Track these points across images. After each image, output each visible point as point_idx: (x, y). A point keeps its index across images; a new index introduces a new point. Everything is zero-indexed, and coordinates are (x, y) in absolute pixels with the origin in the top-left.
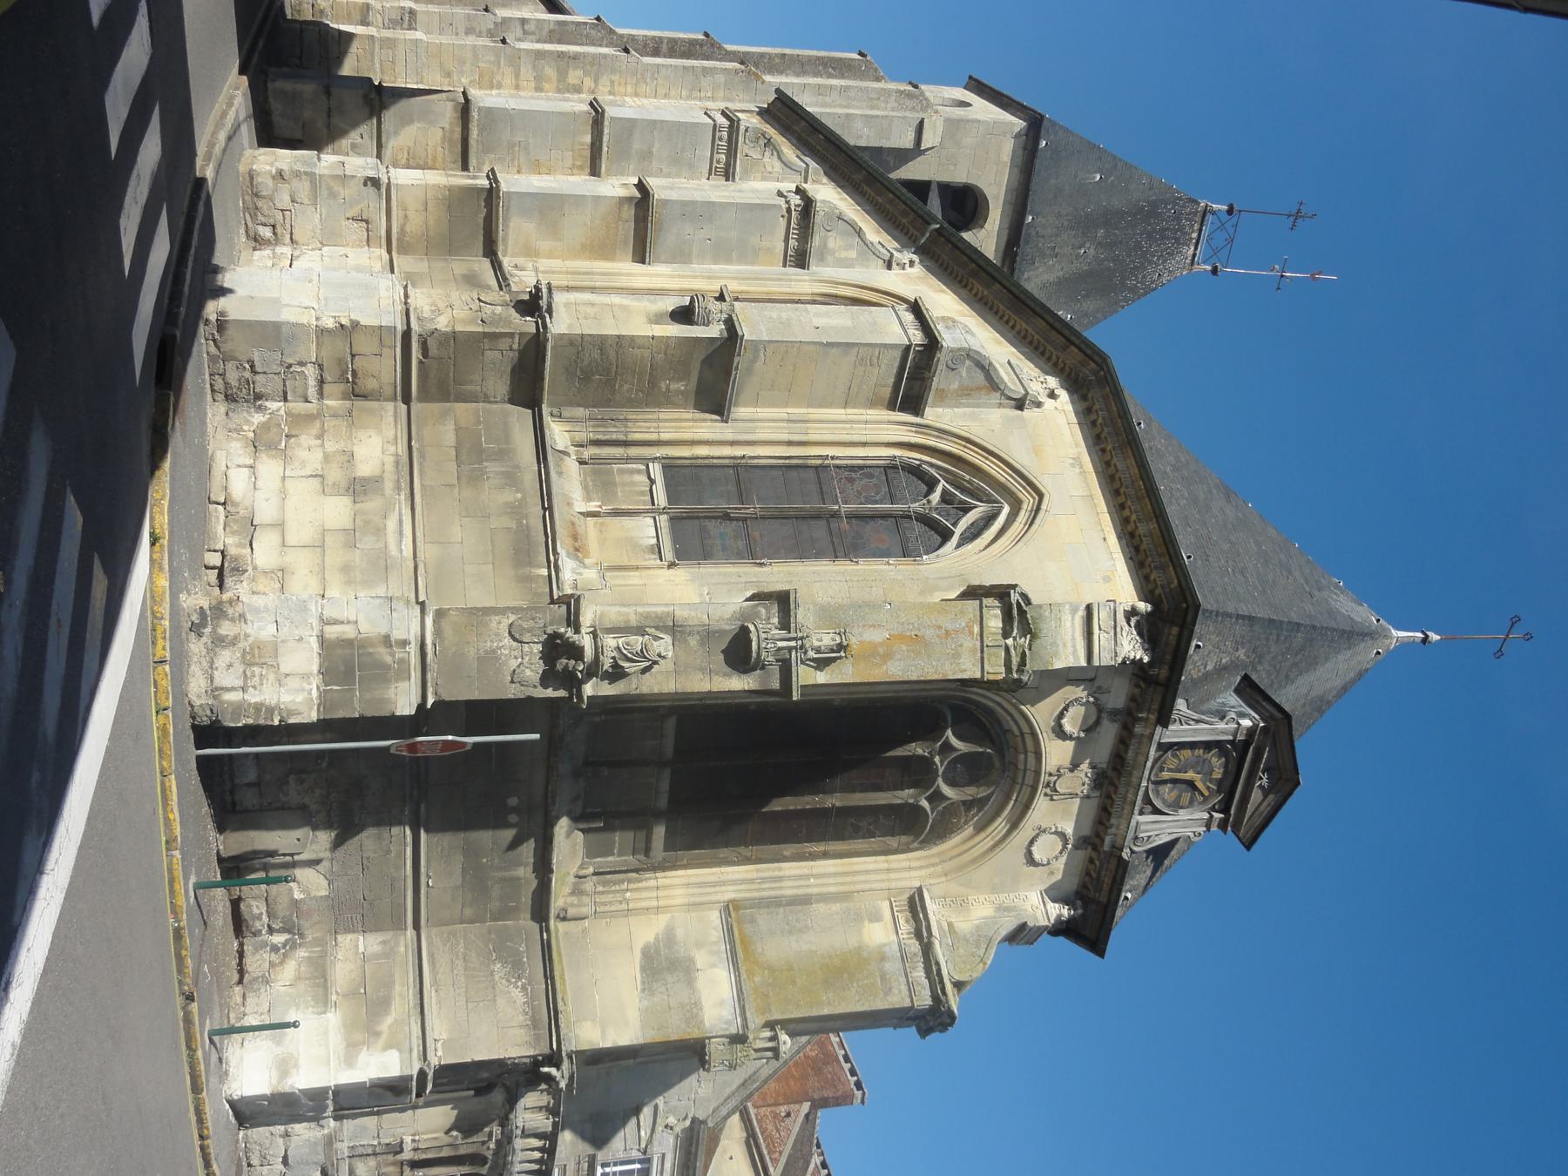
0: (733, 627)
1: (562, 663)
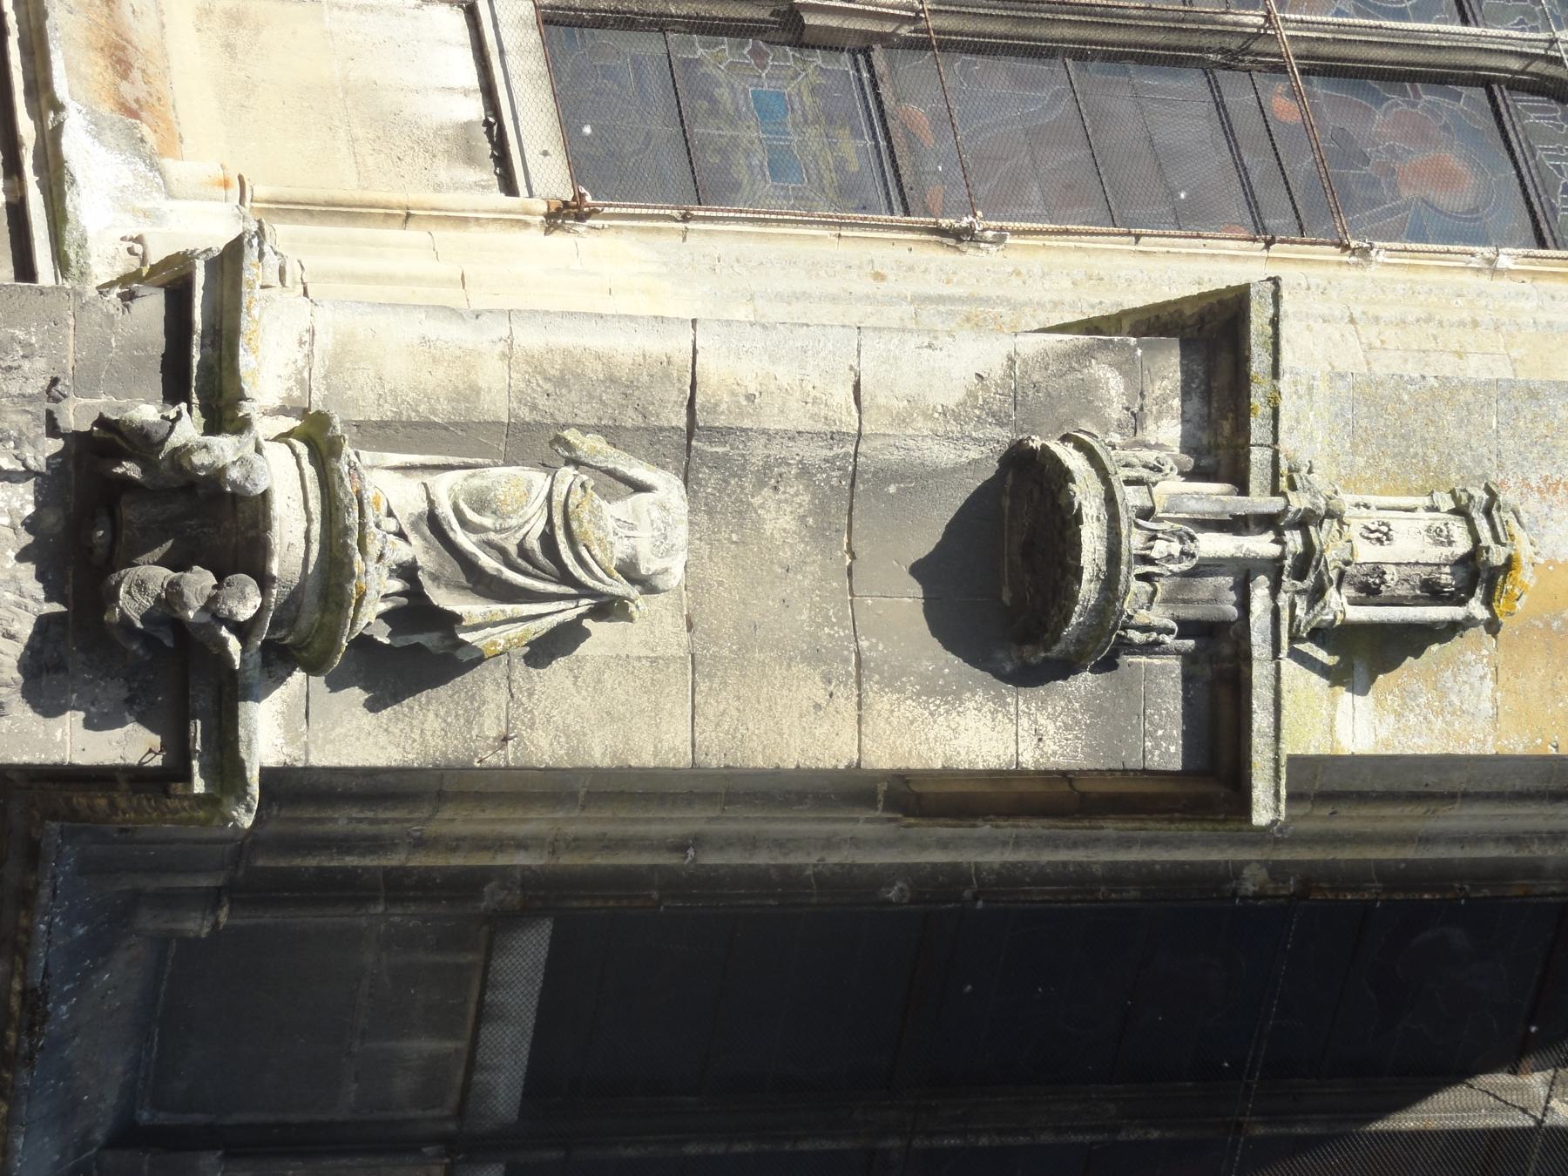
0: (972, 457)
1: (141, 586)
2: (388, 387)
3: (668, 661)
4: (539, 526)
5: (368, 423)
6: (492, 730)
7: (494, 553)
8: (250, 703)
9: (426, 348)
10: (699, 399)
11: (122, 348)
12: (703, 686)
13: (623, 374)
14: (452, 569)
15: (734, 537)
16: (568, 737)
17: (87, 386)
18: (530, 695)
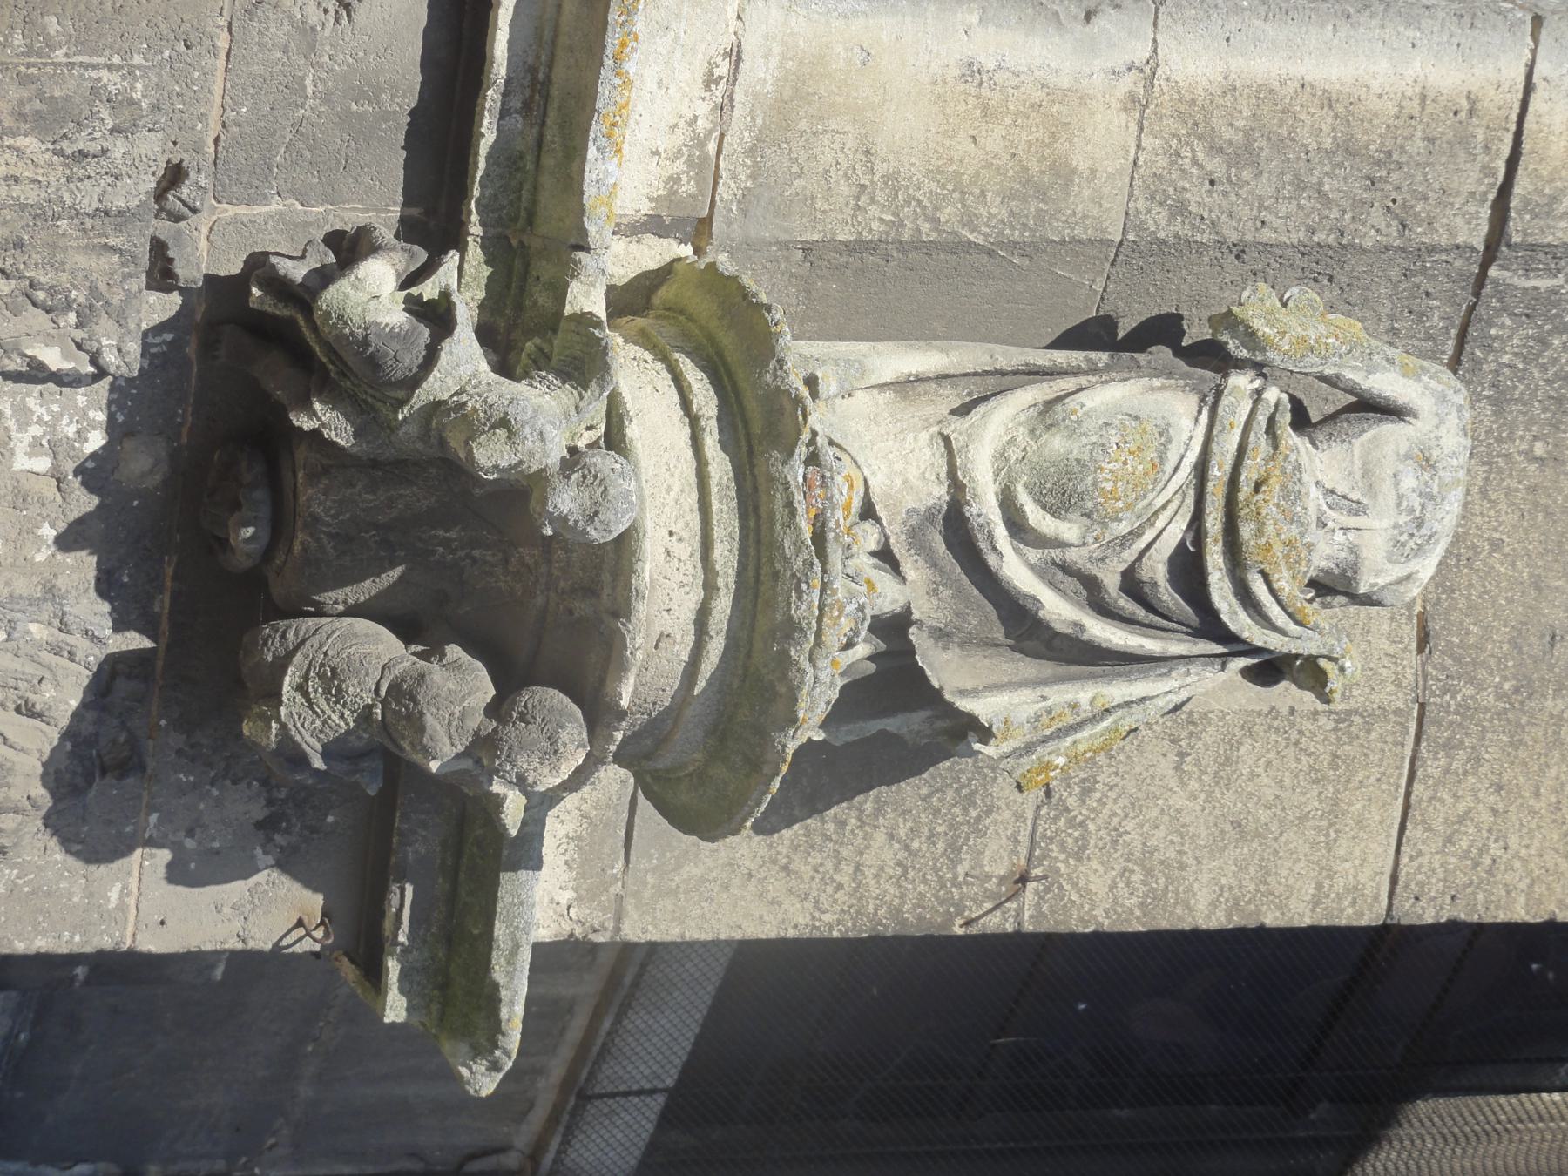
2: (880, 170)
3: (1370, 718)
4: (1176, 532)
5: (832, 245)
6: (997, 859)
7: (1072, 584)
8: (523, 874)
9: (971, 87)
10: (1521, 187)
11: (326, 98)
12: (1432, 767)
13: (1373, 139)
14: (983, 616)
15: (1539, 449)
16: (1148, 872)
17: (245, 174)
18: (1086, 792)
